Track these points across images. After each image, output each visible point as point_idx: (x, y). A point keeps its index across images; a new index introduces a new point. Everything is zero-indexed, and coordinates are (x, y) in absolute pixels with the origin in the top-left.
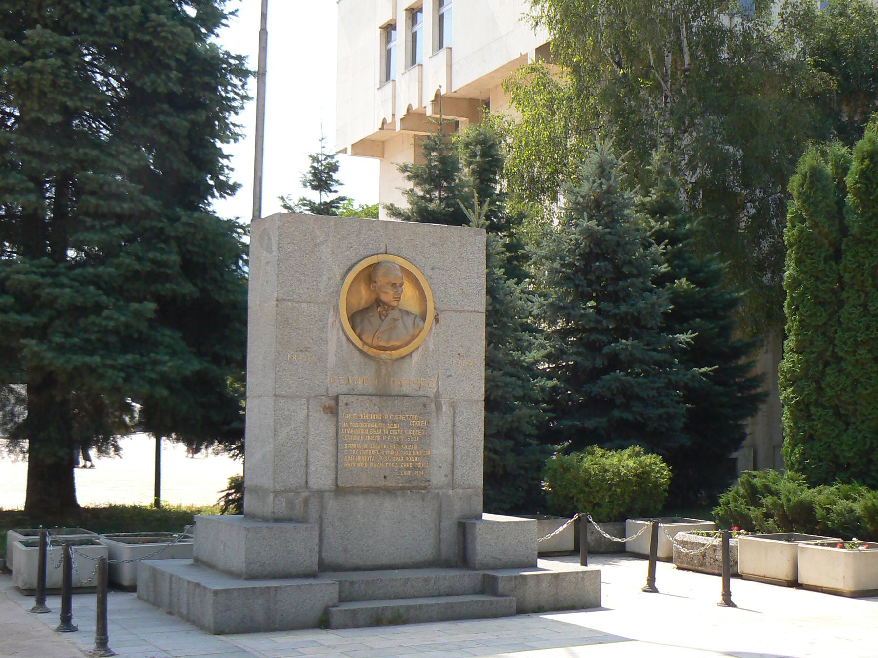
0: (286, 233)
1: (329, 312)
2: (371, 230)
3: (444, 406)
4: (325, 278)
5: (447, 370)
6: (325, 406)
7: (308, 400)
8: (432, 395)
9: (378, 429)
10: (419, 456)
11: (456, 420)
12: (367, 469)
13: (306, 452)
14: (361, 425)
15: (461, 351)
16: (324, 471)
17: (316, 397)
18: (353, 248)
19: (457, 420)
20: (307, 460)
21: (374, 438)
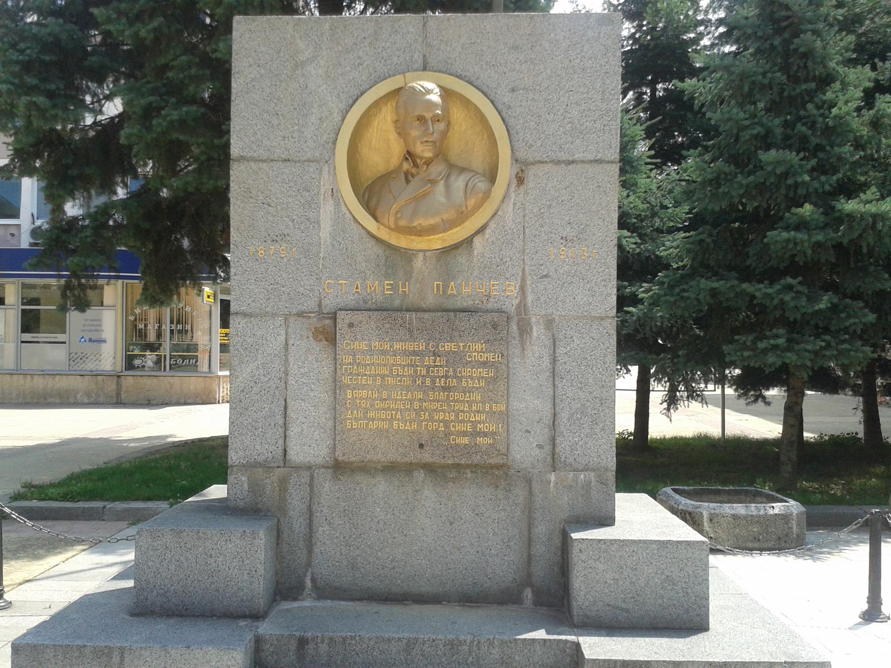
0: (246, 49)
2: (396, 32)
4: (313, 119)
9: (408, 366)
11: (557, 351)
13: (284, 403)
15: (567, 232)
17: (300, 314)
18: (364, 66)
19: (560, 351)
20: (285, 416)
21: (400, 381)
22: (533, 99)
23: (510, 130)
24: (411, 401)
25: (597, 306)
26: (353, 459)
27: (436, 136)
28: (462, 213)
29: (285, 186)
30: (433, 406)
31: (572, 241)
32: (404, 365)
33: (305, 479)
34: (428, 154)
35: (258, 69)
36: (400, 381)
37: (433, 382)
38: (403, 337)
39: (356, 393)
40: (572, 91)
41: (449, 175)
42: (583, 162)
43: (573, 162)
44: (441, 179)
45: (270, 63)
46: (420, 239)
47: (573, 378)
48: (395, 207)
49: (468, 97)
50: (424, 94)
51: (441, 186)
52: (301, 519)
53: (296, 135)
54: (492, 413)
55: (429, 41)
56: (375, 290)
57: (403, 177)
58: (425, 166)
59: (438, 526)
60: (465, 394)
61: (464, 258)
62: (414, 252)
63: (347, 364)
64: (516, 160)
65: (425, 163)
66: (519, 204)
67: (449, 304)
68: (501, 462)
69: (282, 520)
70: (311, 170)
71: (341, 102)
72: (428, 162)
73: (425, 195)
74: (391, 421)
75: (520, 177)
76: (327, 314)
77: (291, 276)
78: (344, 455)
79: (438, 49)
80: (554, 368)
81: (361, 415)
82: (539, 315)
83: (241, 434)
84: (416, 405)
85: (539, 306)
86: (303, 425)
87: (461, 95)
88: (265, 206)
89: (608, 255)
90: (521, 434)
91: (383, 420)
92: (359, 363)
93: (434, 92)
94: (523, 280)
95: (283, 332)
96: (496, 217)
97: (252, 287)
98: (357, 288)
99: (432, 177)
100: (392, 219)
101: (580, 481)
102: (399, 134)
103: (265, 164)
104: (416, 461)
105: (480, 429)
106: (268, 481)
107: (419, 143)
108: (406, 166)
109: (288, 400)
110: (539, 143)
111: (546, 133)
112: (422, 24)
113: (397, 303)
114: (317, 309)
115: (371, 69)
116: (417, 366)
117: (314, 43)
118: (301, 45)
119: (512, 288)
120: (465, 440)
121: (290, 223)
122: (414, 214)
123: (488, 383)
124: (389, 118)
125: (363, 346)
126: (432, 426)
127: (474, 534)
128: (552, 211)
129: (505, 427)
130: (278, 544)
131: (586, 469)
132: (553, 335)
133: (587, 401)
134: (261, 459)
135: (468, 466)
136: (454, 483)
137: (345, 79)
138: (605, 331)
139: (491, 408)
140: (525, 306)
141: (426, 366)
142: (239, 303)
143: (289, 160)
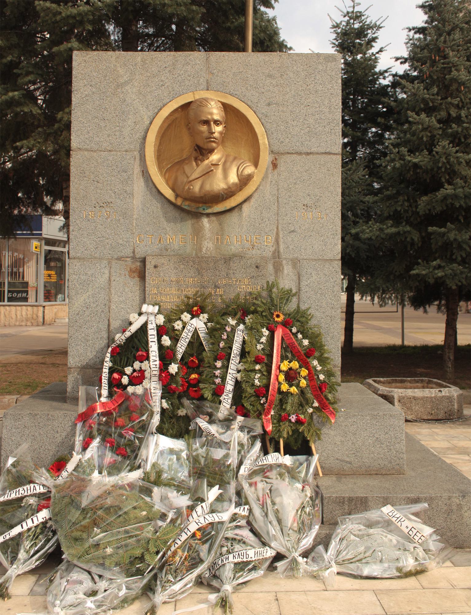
2: (188, 64)
3: (285, 267)
5: (290, 224)
11: (302, 284)
13: (107, 322)
15: (307, 201)
17: (119, 259)
31: (311, 208)
42: (318, 153)
53: (117, 133)
64: (272, 152)
66: (274, 182)
71: (149, 111)
75: (275, 164)
76: (139, 258)
79: (217, 76)
88: (95, 182)
94: (277, 234)
95: (107, 272)
109: (111, 320)
110: (287, 140)
114: (132, 255)
115: (170, 89)
118: (121, 71)
132: (298, 273)
140: (278, 252)
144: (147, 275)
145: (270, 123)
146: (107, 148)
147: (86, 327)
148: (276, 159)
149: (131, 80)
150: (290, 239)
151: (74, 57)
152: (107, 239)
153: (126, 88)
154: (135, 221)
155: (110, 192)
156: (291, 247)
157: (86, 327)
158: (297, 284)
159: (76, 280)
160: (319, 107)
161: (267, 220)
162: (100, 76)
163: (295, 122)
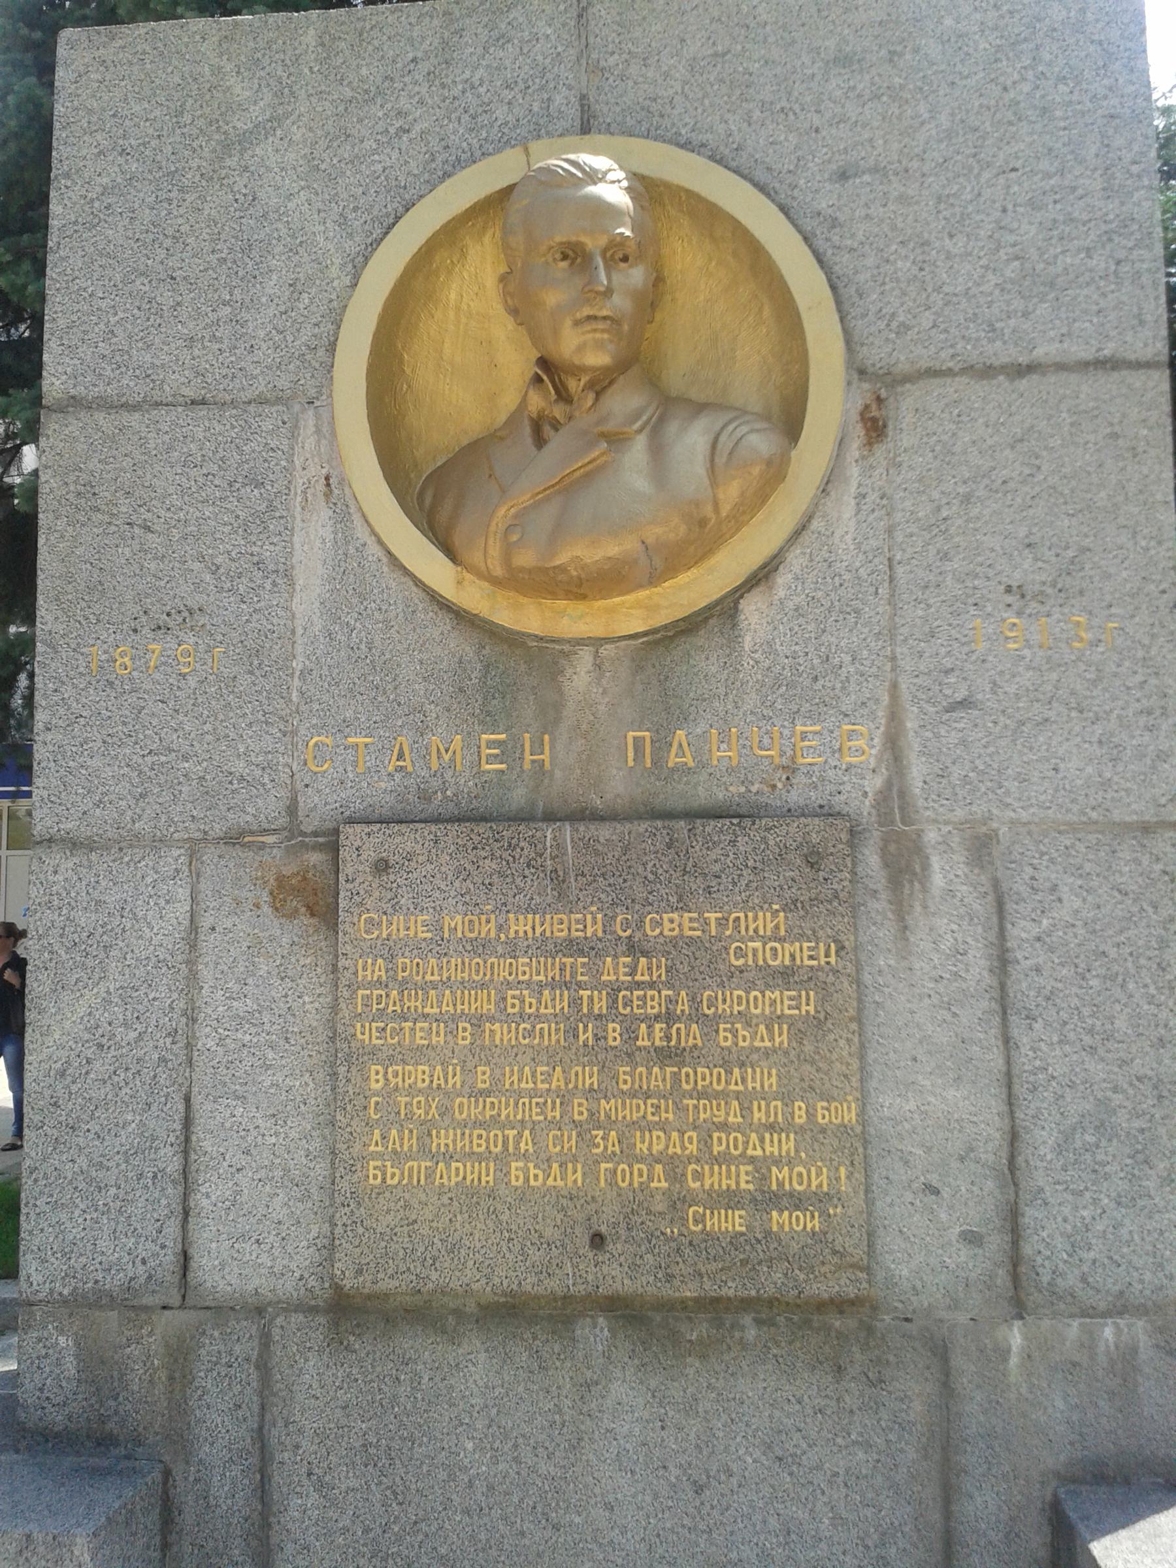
0: (90, 111)
1: (293, 436)
2: (503, 40)
3: (936, 862)
4: (272, 285)
5: (948, 672)
6: (281, 880)
7: (192, 855)
8: (865, 808)
9: (552, 985)
10: (789, 1126)
11: (1013, 932)
12: (492, 1195)
13: (181, 1107)
14: (456, 967)
15: (1024, 570)
16: (277, 1202)
17: (235, 839)
18: (413, 135)
19: (1020, 931)
20: (186, 1147)
21: (530, 1033)
22: (902, 199)
23: (840, 285)
24: (565, 1099)
25: (1128, 791)
26: (387, 1284)
27: (620, 303)
28: (703, 523)
29: (194, 472)
30: (631, 1111)
31: (1041, 597)
32: (540, 985)
33: (247, 1348)
34: (597, 359)
35: (121, 160)
36: (530, 1033)
37: (630, 1035)
38: (537, 899)
39: (396, 1075)
40: (1014, 170)
41: (662, 420)
42: (1061, 367)
43: (1030, 369)
44: (640, 431)
45: (154, 143)
46: (581, 607)
47: (1064, 1015)
48: (503, 514)
49: (712, 198)
50: (578, 183)
51: (638, 451)
52: (236, 1471)
53: (223, 332)
54: (812, 1133)
55: (594, 56)
56: (453, 760)
57: (527, 430)
58: (591, 396)
59: (656, 1496)
60: (729, 1072)
61: (713, 659)
62: (566, 648)
63: (371, 985)
64: (862, 372)
65: (590, 385)
66: (873, 497)
67: (673, 795)
68: (851, 1292)
69: (178, 1471)
70: (268, 425)
71: (350, 236)
72: (601, 383)
73: (589, 476)
74: (502, 1161)
75: (874, 420)
76: (315, 834)
77: (207, 727)
78: (359, 1272)
79: (623, 78)
80: (1003, 987)
81: (410, 1143)
82: (946, 823)
83: (55, 1206)
84: (580, 1109)
85: (948, 793)
86: (238, 1176)
87: (690, 194)
88: (137, 530)
89: (1153, 636)
90: (909, 1198)
91: (480, 1158)
92: (405, 981)
93: (611, 176)
94: (895, 716)
95: (183, 893)
96: (806, 537)
97: (95, 763)
98: (401, 756)
99: (609, 427)
100: (495, 550)
101: (1102, 1348)
102: (514, 312)
103: (137, 415)
104: (581, 1289)
105: (780, 1184)
106: (134, 1350)
107: (568, 322)
108: (536, 402)
109: (196, 1100)
110: (926, 319)
111: (946, 289)
112: (574, 13)
113: (518, 796)
114: (283, 821)
115: (434, 142)
116: (580, 985)
117: (272, 82)
118: (240, 90)
119: (861, 743)
120: (735, 1221)
121: (208, 577)
122: (558, 534)
123: (798, 1035)
124: (490, 281)
125: (418, 927)
126: (632, 1176)
127: (773, 1522)
128: (975, 511)
129: (859, 1176)
130: (165, 1546)
131: (1121, 1307)
132: (996, 884)
133: (1115, 1090)
134: (113, 1282)
135: (746, 1304)
136: (703, 1357)
137: (359, 172)
138: (1158, 867)
139: (811, 1115)
140: (902, 794)
141: (605, 985)
142: (60, 810)
143: (203, 402)
144: (343, 904)
145: (852, 250)
146: (186, 391)
147: (94, 1127)
148: (879, 400)
149: (276, 120)
150: (954, 737)
151: (62, 51)
152: (186, 758)
153: (258, 151)
154: (296, 682)
155: (196, 566)
156: (957, 772)
157: (94, 1127)
158: (992, 936)
159: (56, 932)
160: (1062, 173)
161: (847, 659)
162: (157, 113)
163: (961, 240)
